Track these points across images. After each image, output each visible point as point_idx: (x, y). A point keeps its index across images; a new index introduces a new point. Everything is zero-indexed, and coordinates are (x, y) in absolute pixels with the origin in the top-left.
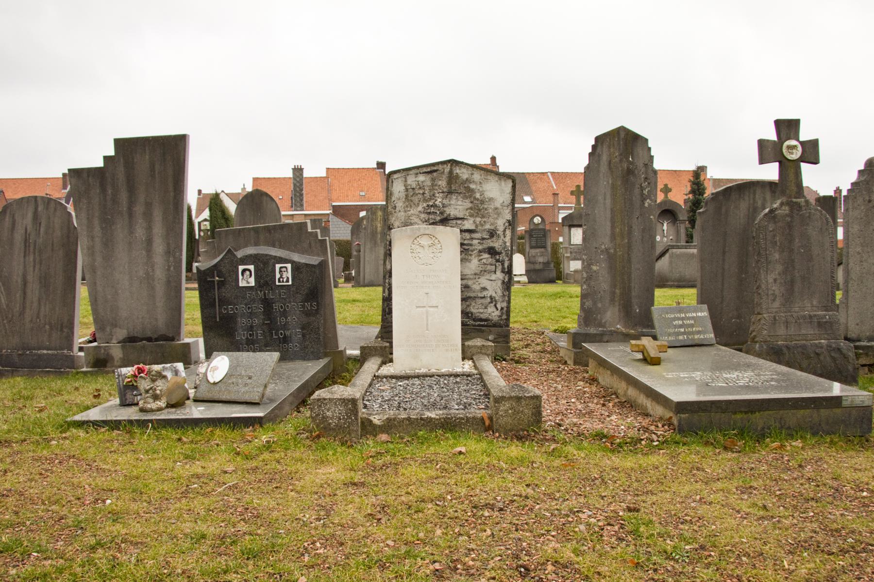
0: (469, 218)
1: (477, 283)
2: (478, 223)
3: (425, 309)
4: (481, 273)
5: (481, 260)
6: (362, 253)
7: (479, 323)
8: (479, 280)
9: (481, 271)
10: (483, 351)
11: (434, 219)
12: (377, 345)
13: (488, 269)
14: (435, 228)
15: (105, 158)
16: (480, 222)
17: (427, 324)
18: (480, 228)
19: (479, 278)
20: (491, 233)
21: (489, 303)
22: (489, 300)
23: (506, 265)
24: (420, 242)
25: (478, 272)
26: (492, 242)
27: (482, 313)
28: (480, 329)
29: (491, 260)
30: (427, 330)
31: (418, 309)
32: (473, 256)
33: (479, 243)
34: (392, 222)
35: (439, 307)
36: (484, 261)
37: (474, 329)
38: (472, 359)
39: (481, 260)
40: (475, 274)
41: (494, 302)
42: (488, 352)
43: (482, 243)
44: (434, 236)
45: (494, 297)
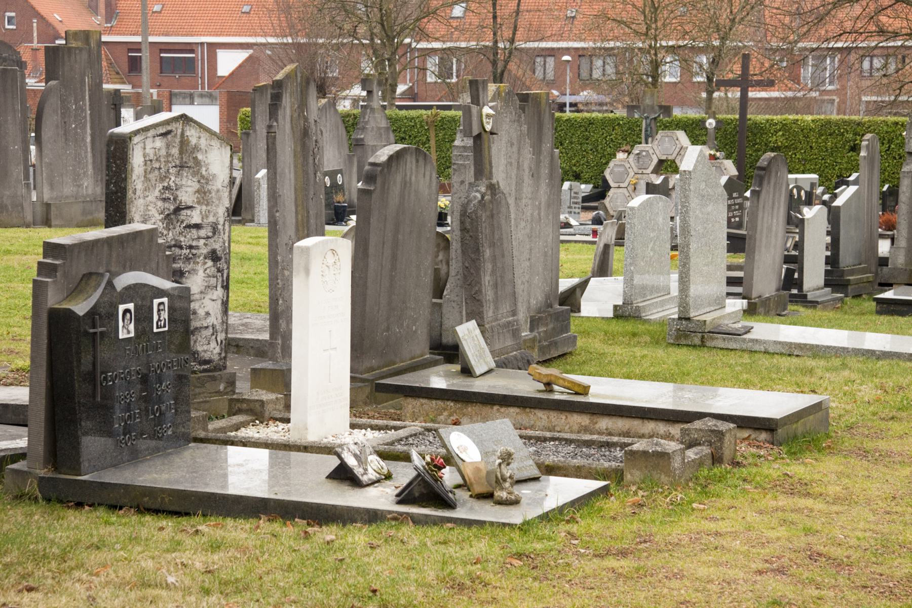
0: (196, 206)
15: (615, 307)
23: (225, 275)
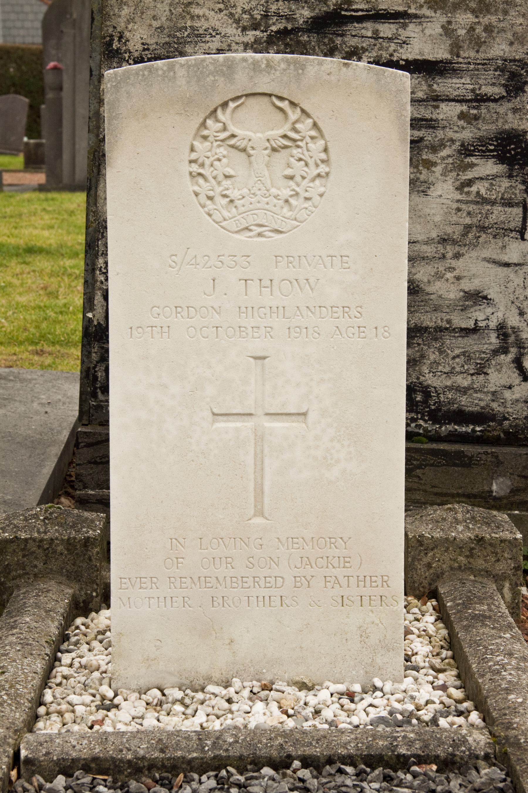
1: (449, 275)
2: (462, 32)
3: (250, 423)
4: (465, 235)
5: (470, 183)
6: (66, 94)
7: (450, 427)
8: (459, 264)
9: (468, 228)
10: (480, 563)
11: (289, 18)
12: (53, 532)
13: (493, 218)
14: (303, 67)
16: (472, 29)
17: (259, 491)
18: (468, 53)
19: (457, 256)
20: (513, 75)
21: (496, 352)
22: (494, 339)
24: (233, 129)
25: (456, 232)
26: (515, 110)
27: (464, 391)
28: (459, 455)
29: (505, 183)
30: (260, 512)
31: (222, 425)
32: (438, 169)
33: (462, 116)
34: (121, 25)
35: (312, 416)
36: (481, 187)
37: (434, 453)
38: (434, 594)
39: (470, 183)
40: (444, 240)
41: (513, 350)
42: (501, 567)
43: (476, 118)
44: (293, 104)
45: (516, 330)
